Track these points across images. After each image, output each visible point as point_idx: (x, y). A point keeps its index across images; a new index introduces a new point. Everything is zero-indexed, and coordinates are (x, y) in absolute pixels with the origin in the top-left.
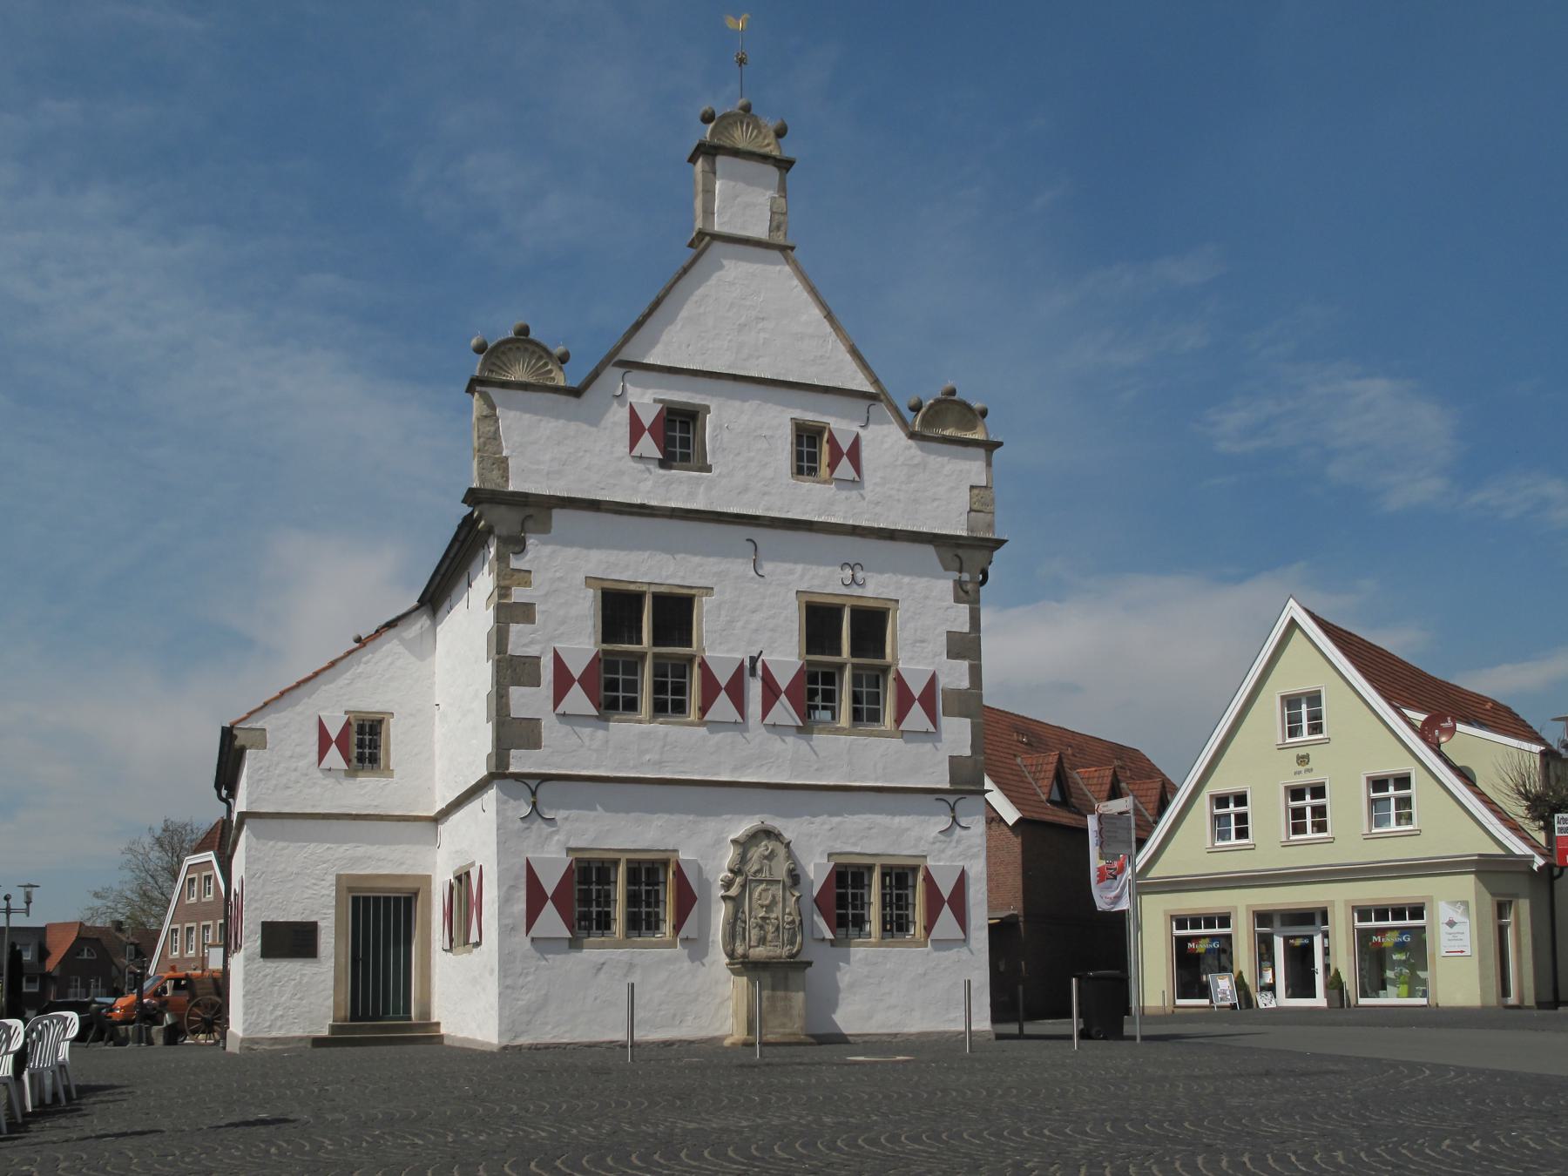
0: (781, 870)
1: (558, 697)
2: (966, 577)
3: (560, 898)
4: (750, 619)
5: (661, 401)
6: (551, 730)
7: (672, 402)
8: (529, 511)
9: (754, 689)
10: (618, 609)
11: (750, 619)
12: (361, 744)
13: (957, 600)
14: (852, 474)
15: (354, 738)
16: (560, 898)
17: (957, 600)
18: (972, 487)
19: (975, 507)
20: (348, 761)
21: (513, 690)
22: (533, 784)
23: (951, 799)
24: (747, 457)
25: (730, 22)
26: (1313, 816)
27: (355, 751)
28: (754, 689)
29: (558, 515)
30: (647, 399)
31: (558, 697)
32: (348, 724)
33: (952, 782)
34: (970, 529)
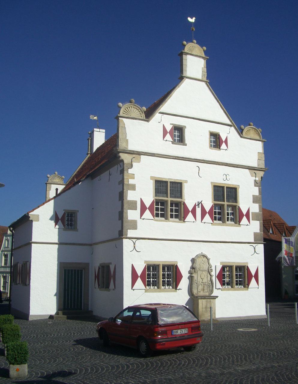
0: (206, 267)
1: (142, 213)
2: (257, 179)
3: (143, 277)
4: (198, 193)
5: (172, 124)
6: (140, 223)
7: (175, 125)
8: (134, 156)
9: (199, 211)
10: (161, 186)
11: (198, 193)
12: (68, 221)
13: (255, 186)
14: (226, 148)
15: (66, 218)
16: (143, 277)
17: (255, 186)
18: (258, 152)
19: (259, 159)
20: (64, 226)
21: (266, 318)
22: (134, 240)
23: (254, 245)
24: (197, 141)
25: (189, 19)
26: (147, 282)
27: (66, 223)
28: (199, 211)
29: (142, 157)
30: (169, 123)
31: (142, 213)
32: (64, 214)
33: (255, 240)
34: (258, 165)
